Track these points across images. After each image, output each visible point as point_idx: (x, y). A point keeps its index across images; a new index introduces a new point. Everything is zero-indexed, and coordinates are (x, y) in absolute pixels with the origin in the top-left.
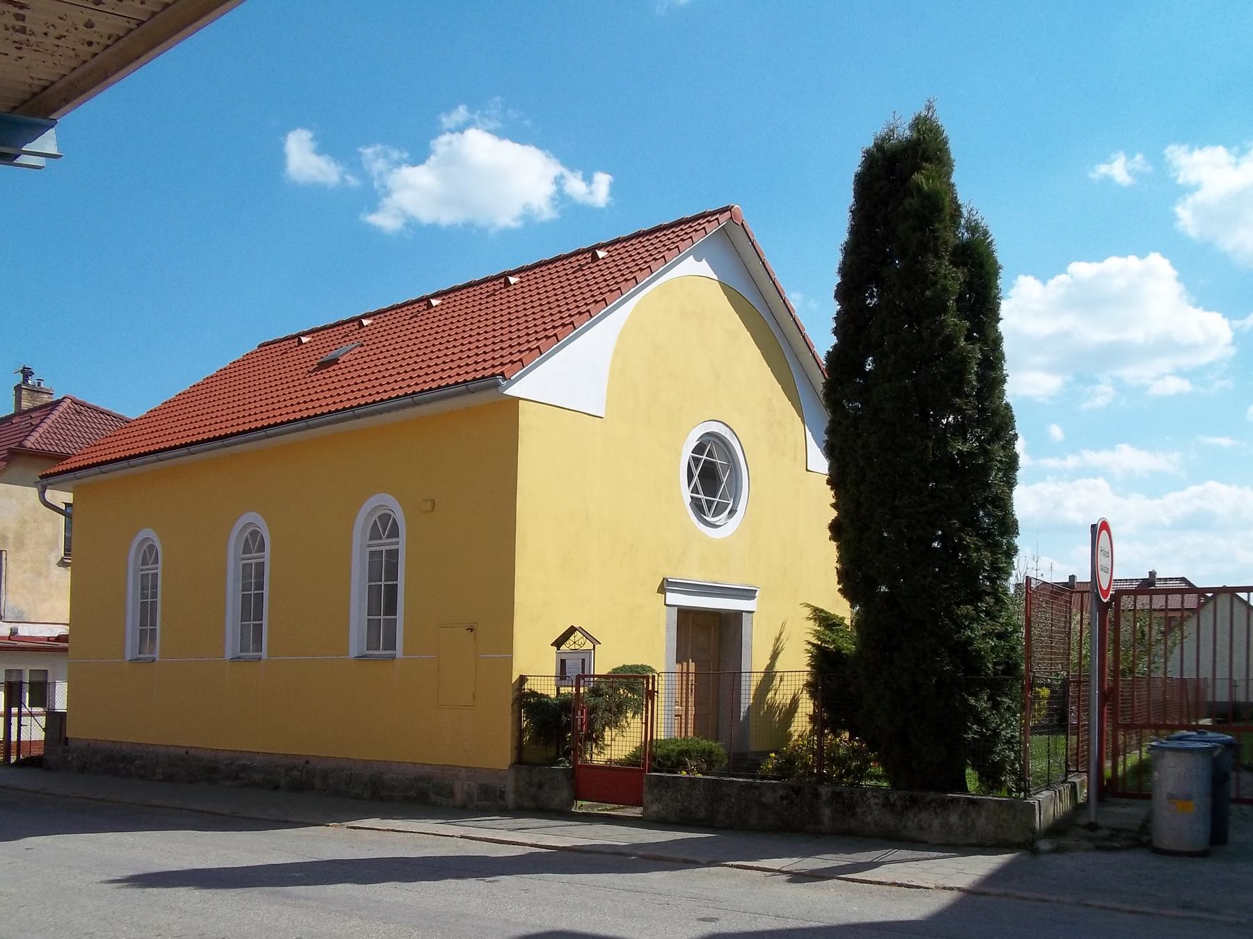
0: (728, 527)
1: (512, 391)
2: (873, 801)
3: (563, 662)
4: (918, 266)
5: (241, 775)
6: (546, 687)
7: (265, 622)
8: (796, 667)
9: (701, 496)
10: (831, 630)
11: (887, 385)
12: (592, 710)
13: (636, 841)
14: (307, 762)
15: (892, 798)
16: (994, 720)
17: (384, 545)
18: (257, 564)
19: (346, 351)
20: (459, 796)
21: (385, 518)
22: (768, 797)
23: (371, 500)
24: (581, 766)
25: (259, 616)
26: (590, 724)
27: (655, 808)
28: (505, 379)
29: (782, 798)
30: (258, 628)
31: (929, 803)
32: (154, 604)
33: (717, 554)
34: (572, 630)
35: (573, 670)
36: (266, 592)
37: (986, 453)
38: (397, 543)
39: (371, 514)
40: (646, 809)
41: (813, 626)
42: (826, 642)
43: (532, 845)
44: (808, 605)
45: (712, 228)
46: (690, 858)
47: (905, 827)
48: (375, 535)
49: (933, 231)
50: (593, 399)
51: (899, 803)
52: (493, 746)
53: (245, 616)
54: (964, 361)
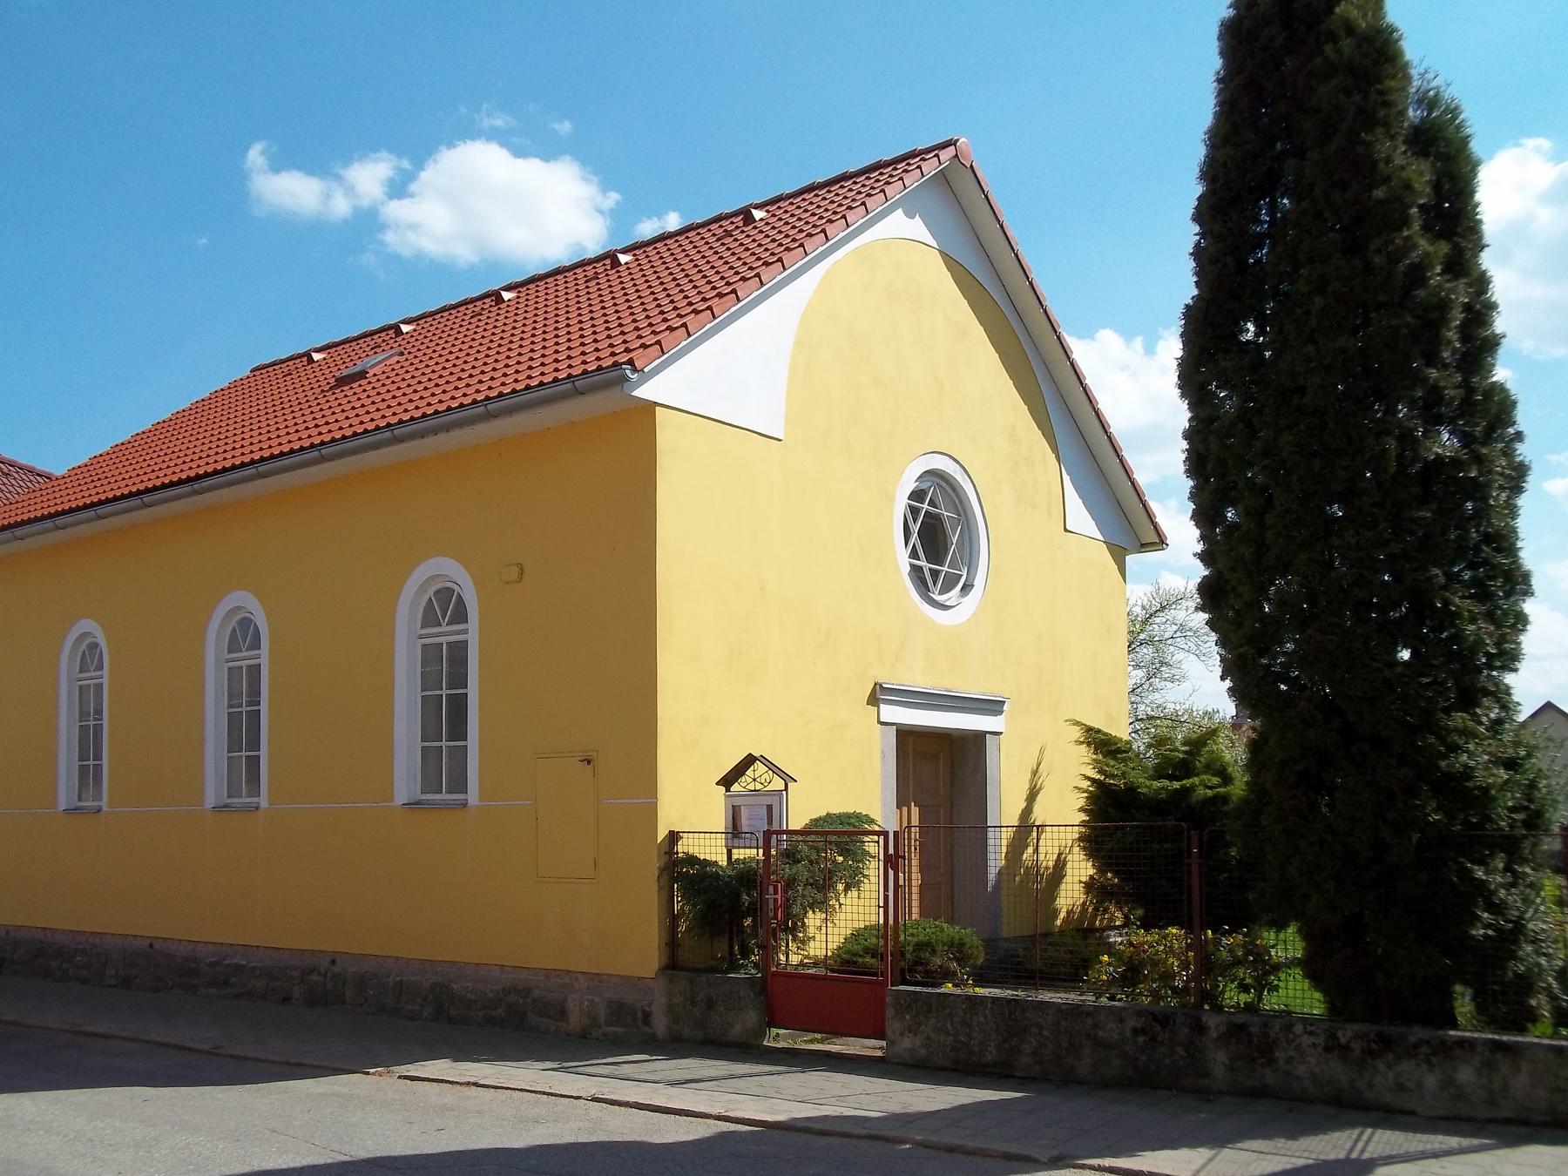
0: (963, 609)
1: (645, 392)
2: (1306, 1040)
3: (735, 814)
4: (1360, 149)
5: (233, 980)
6: (713, 850)
7: (264, 753)
8: (1064, 811)
9: (923, 563)
10: (1115, 759)
11: (1310, 348)
12: (790, 883)
13: (896, 1108)
14: (333, 962)
15: (1344, 1036)
16: (1512, 898)
17: (445, 634)
18: (249, 667)
19: (375, 363)
20: (575, 1020)
21: (445, 595)
22: (1110, 1031)
23: (421, 568)
24: (774, 974)
25: (255, 744)
26: (787, 906)
27: (907, 1042)
28: (635, 370)
29: (1136, 1032)
30: (254, 763)
31: (1416, 1046)
32: (98, 729)
33: (949, 647)
34: (750, 760)
35: (752, 821)
36: (264, 708)
37: (1478, 459)
38: (465, 632)
39: (423, 588)
40: (891, 1043)
41: (1085, 754)
42: (1113, 776)
43: (719, 1118)
44: (1077, 723)
45: (930, 167)
46: (1014, 1149)
47: (1370, 1086)
48: (430, 619)
49: (1381, 93)
50: (765, 410)
51: (1357, 1046)
52: (629, 939)
53: (234, 745)
54: (1444, 306)
